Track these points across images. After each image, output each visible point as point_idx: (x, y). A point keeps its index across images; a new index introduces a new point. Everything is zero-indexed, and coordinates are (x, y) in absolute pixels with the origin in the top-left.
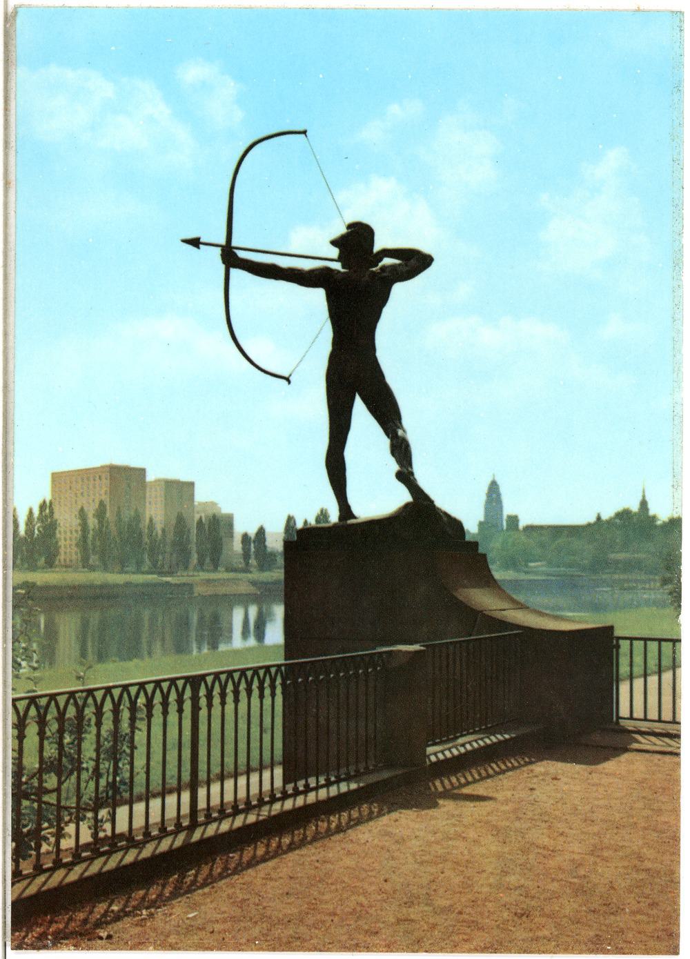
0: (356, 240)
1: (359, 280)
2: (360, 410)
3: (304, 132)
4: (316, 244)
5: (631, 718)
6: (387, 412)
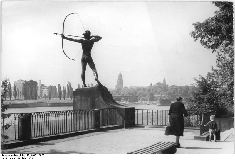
0: (87, 34)
1: (88, 42)
2: (88, 66)
3: (77, 13)
5: (137, 124)
6: (93, 67)
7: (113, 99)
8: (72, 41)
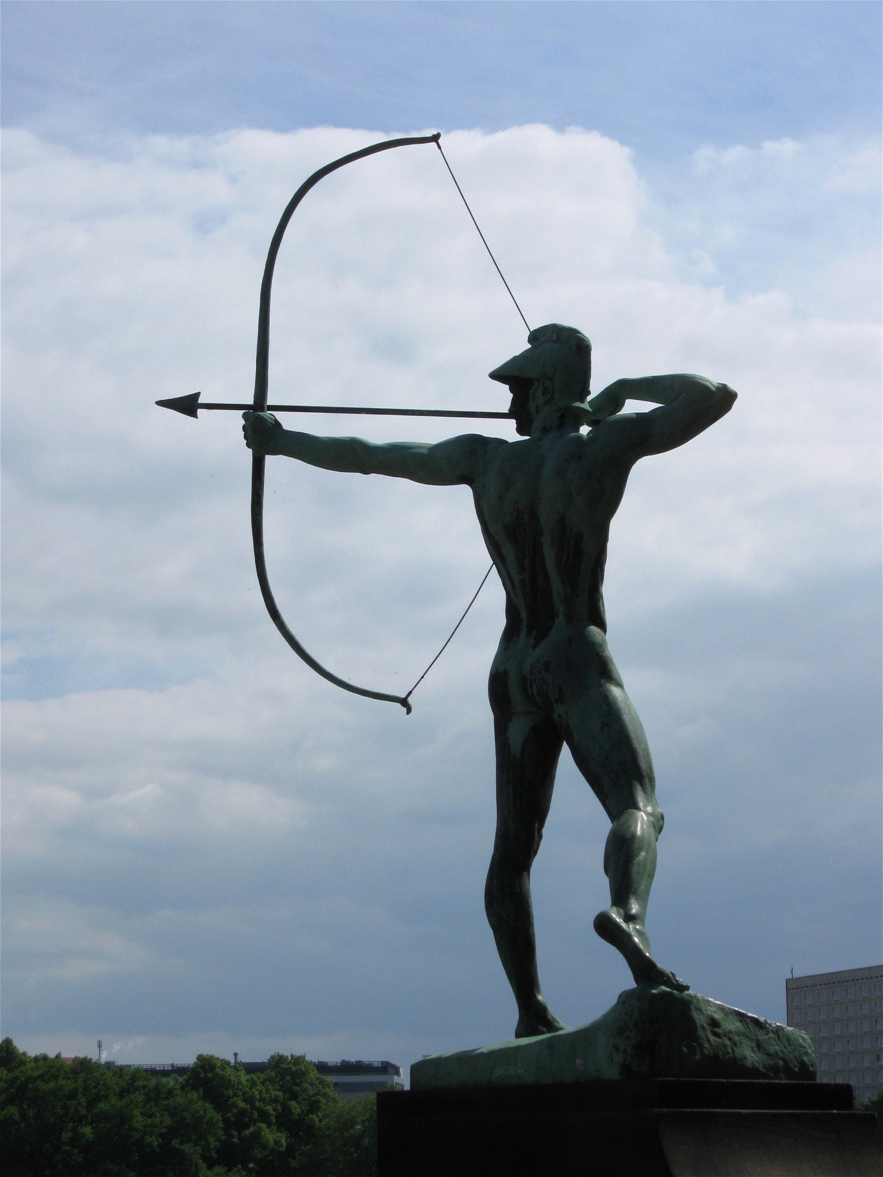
0: (549, 368)
3: (435, 138)
6: (620, 773)
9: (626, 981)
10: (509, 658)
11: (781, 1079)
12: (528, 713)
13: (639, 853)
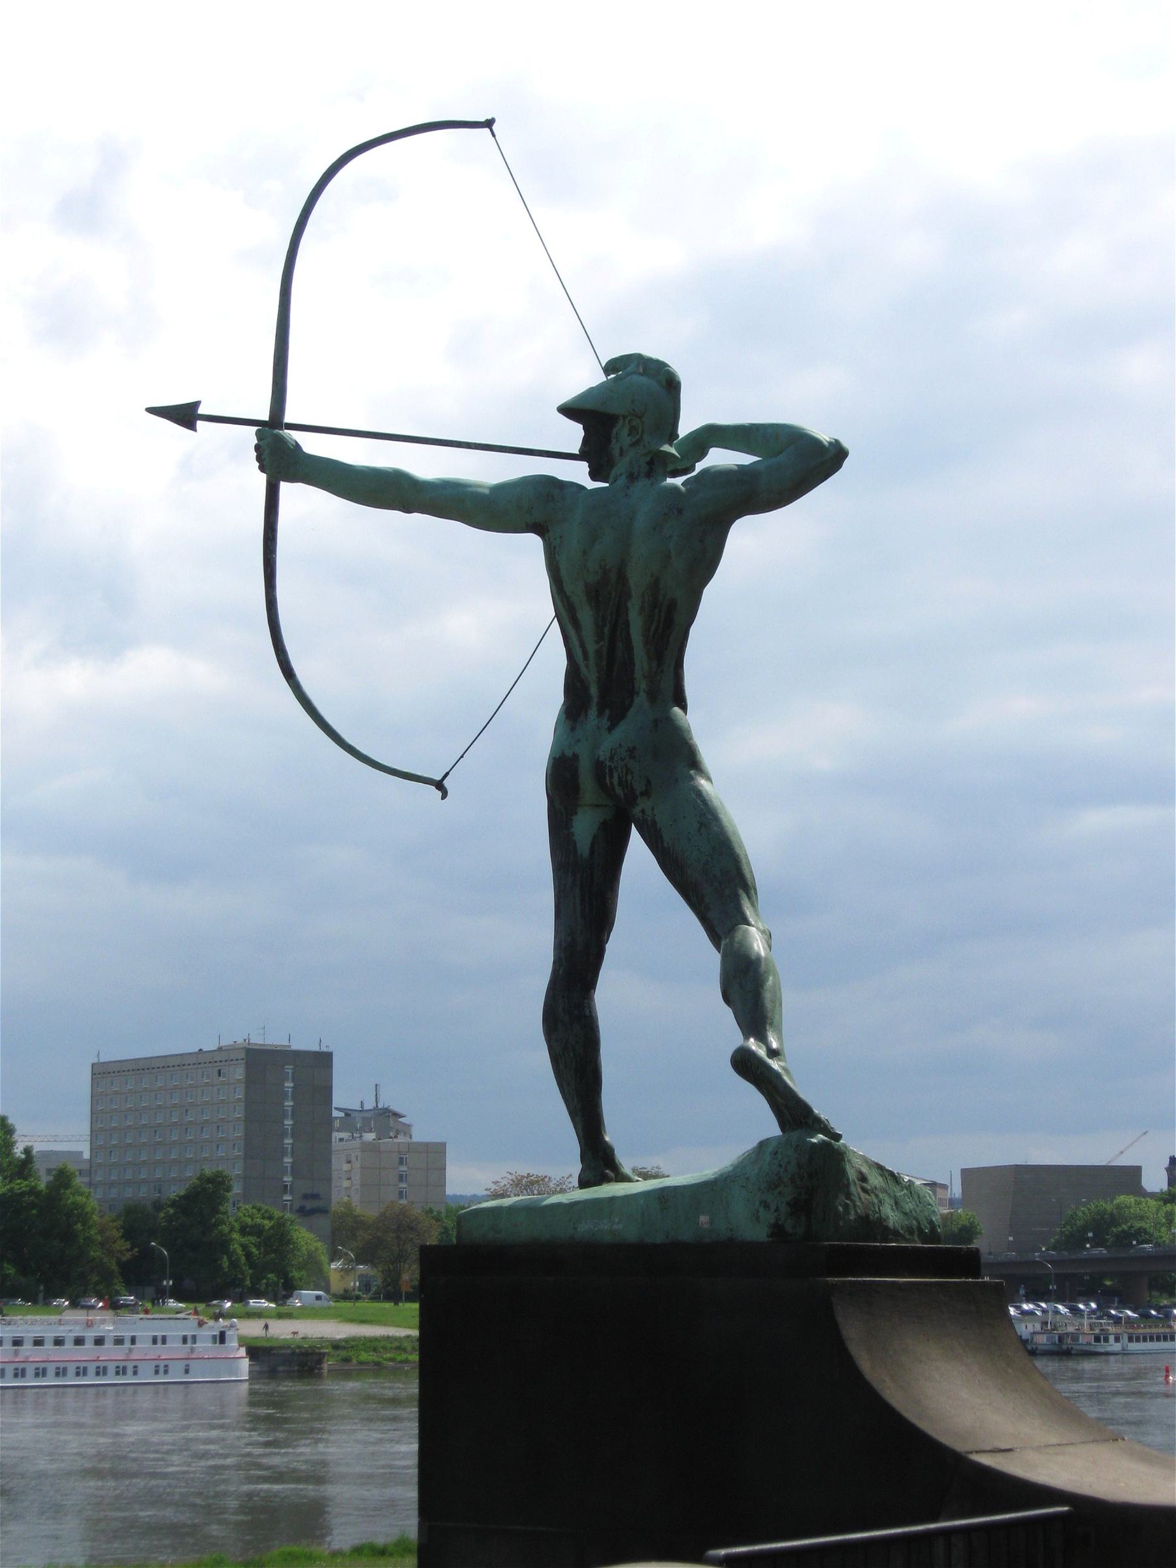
3: (489, 124)
4: (515, 404)
6: (714, 881)
7: (420, 1360)
8: (407, 508)
9: (768, 1126)
10: (579, 741)
11: (915, 1242)
12: (597, 806)
13: (767, 980)
